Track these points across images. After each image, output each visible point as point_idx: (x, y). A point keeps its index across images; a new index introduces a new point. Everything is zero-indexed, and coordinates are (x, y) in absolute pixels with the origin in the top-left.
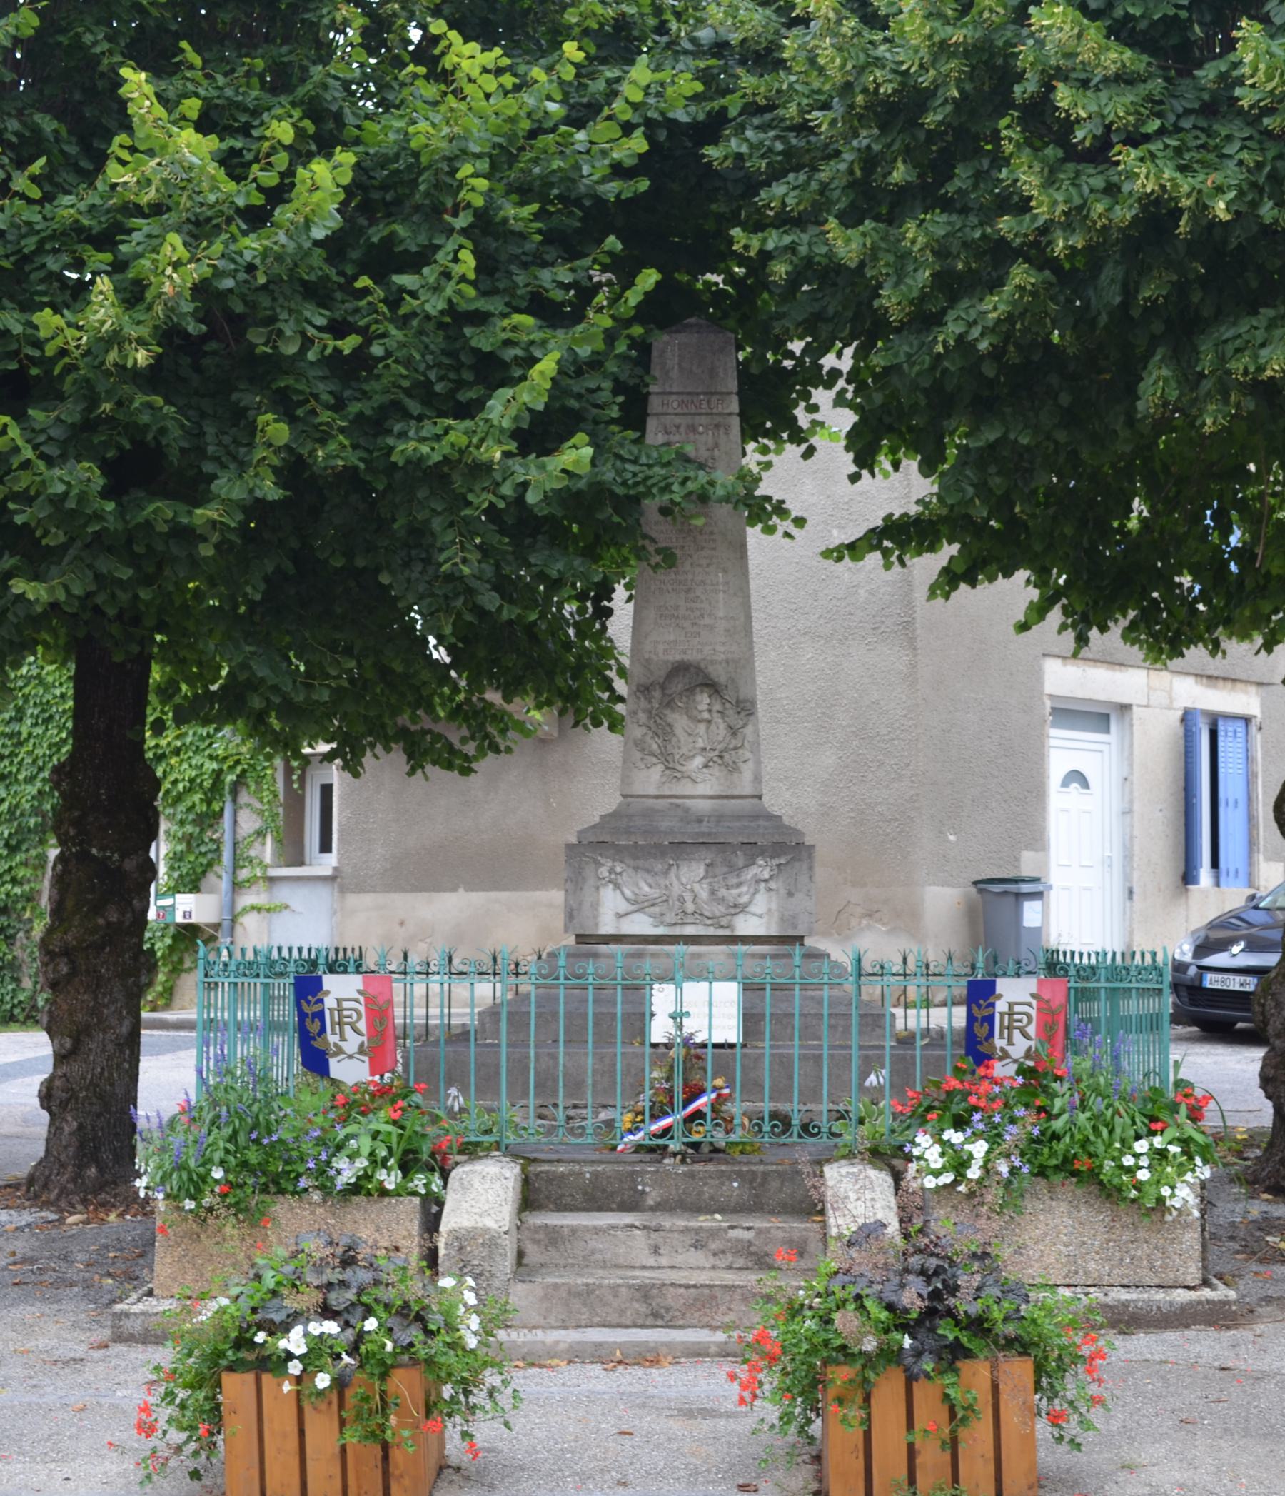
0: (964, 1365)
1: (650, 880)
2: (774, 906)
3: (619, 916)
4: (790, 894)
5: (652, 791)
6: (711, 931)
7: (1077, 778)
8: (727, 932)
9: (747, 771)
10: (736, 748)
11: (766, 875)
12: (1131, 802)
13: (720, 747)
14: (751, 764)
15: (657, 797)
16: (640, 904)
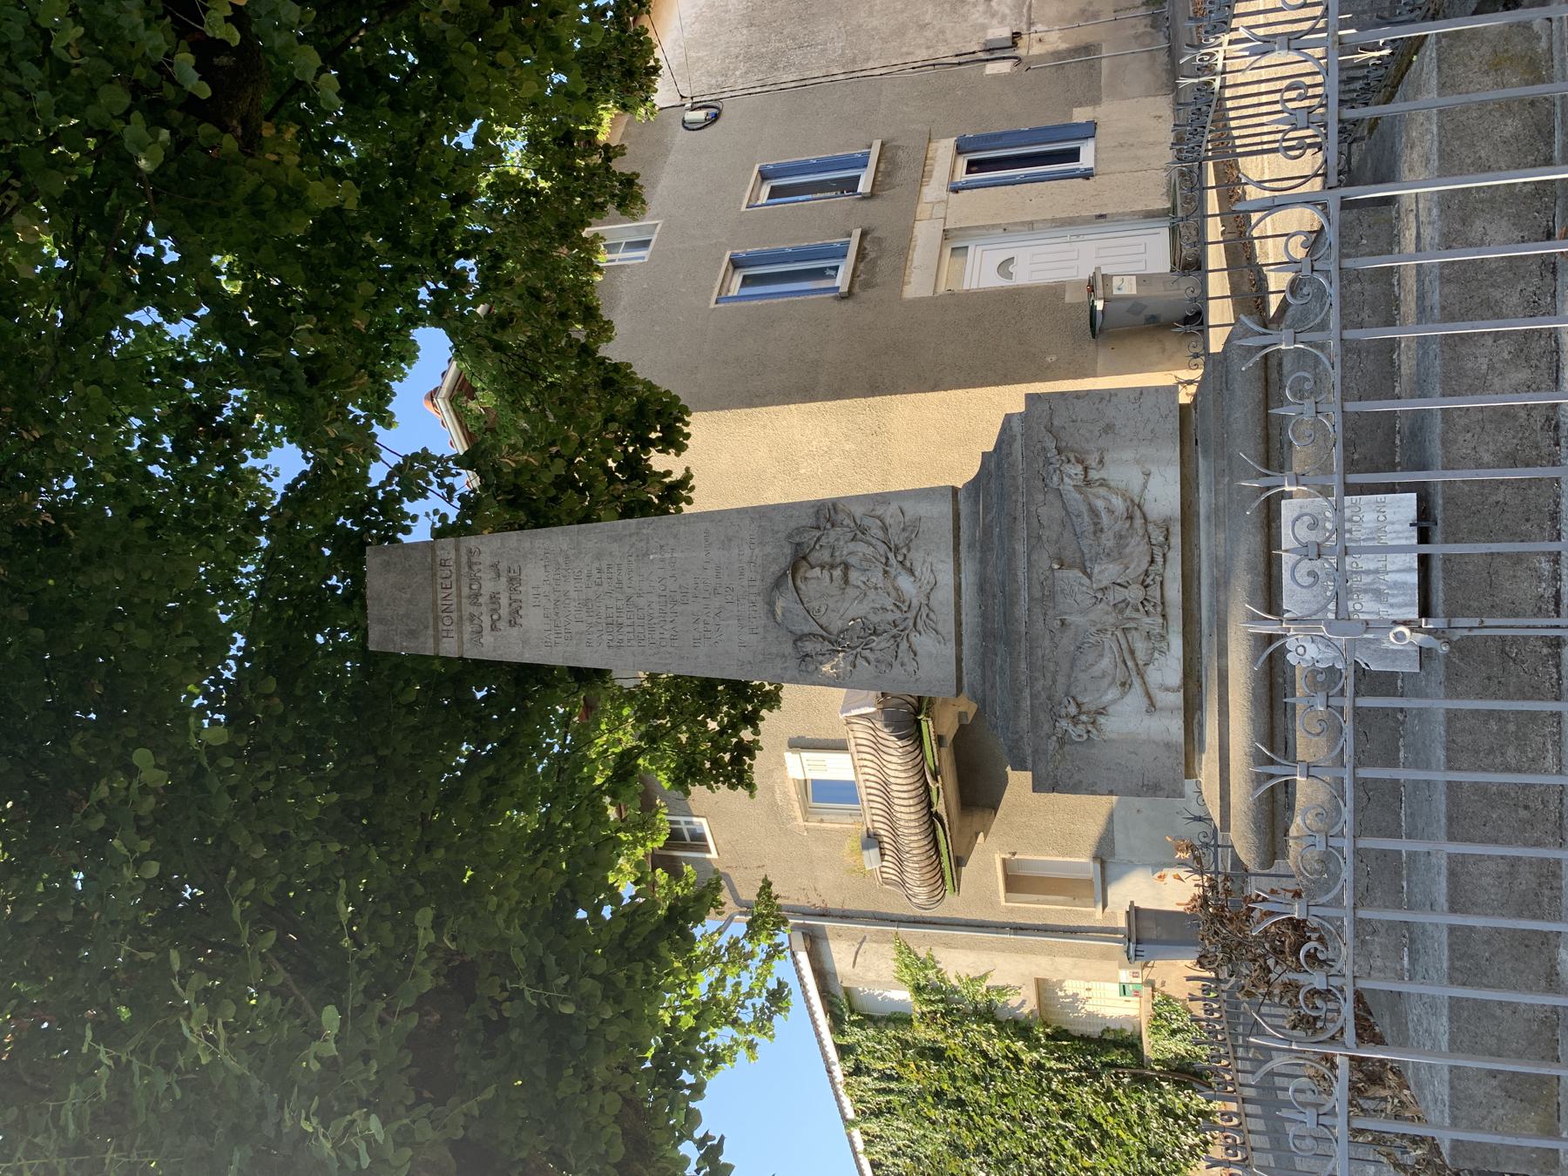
1: (1091, 658)
2: (1128, 455)
3: (1152, 706)
4: (1109, 429)
5: (950, 650)
6: (1175, 556)
7: (1004, 267)
8: (1176, 529)
9: (923, 509)
10: (885, 529)
12: (1023, 223)
13: (882, 548)
14: (907, 506)
15: (959, 642)
16: (1132, 672)
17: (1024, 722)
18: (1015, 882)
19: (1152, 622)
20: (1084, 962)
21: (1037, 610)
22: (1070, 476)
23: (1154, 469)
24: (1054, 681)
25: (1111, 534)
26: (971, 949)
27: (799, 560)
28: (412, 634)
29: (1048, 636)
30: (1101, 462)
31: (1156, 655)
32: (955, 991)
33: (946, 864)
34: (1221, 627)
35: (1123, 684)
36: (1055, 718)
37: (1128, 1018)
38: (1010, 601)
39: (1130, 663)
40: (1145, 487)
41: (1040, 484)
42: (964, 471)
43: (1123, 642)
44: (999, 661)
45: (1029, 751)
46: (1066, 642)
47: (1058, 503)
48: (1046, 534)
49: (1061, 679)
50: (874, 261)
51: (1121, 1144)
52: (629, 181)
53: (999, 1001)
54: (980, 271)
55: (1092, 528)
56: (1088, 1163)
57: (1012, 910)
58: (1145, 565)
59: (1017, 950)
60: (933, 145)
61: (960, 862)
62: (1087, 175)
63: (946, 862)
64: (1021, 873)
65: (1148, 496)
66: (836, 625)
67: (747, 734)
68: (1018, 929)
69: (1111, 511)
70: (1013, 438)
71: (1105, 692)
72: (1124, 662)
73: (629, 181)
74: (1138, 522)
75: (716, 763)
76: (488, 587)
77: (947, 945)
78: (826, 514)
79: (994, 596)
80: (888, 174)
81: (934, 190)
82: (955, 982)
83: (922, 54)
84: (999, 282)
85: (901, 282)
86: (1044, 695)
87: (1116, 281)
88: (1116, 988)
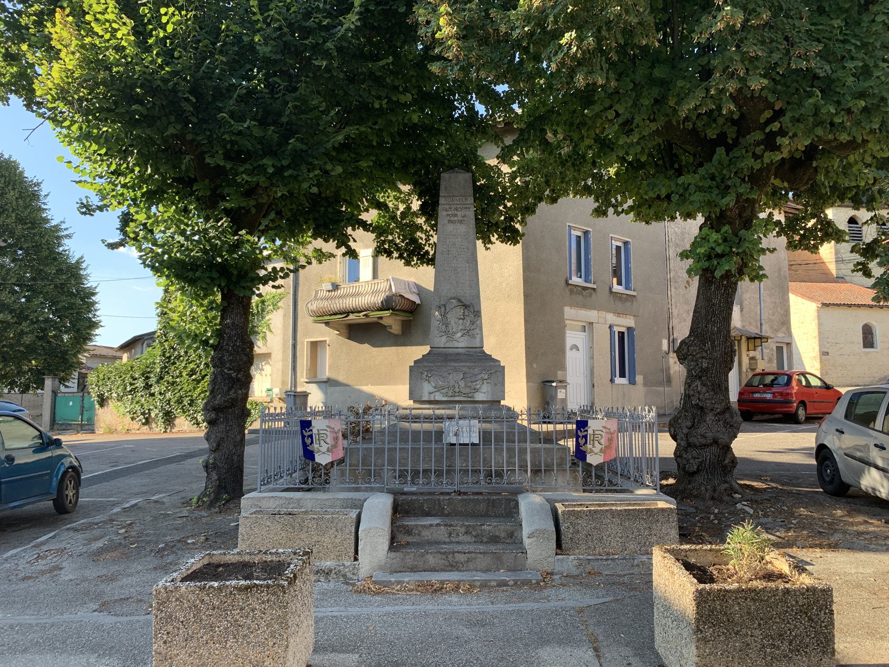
4: (496, 385)
6: (465, 399)
7: (575, 347)
9: (478, 340)
16: (438, 389)
18: (315, 346)
19: (450, 394)
20: (280, 373)
26: (284, 326)
27: (466, 306)
28: (446, 188)
32: (263, 318)
33: (326, 318)
37: (253, 392)
38: (455, 361)
42: (487, 350)
46: (445, 374)
50: (582, 294)
51: (195, 388)
52: (605, 214)
53: (260, 337)
54: (574, 337)
56: (184, 374)
57: (303, 344)
59: (284, 345)
60: (632, 317)
61: (327, 324)
62: (612, 381)
63: (326, 317)
64: (319, 348)
66: (448, 316)
67: (395, 255)
68: (294, 346)
73: (605, 214)
75: (384, 242)
76: (459, 213)
77: (285, 315)
78: (477, 314)
80: (620, 299)
81: (611, 318)
82: (267, 318)
83: (675, 312)
84: (568, 345)
85: (571, 306)
87: (563, 391)
88: (269, 387)
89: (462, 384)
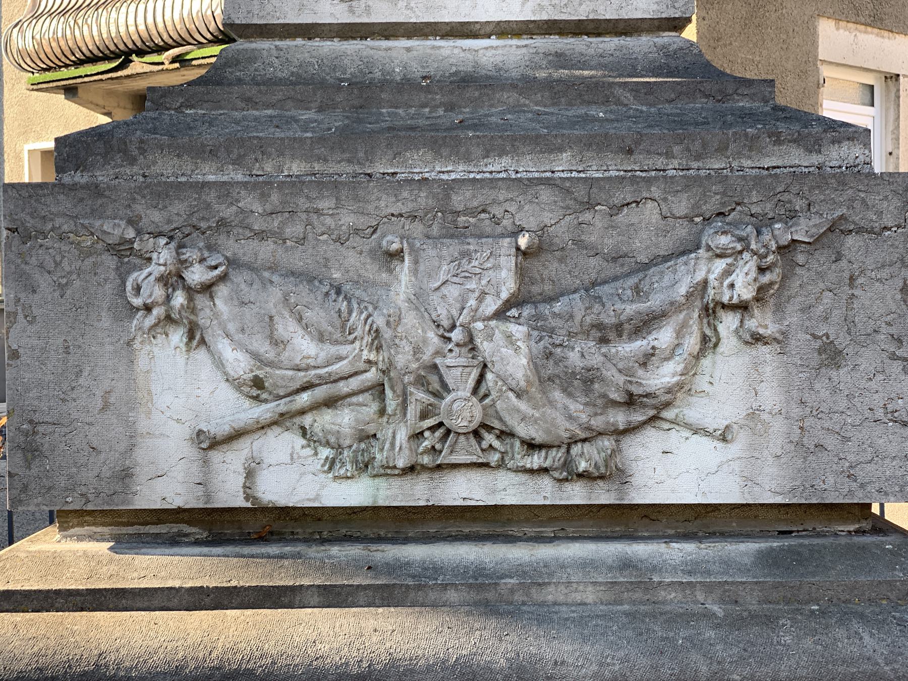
0: (271, 289)
2: (770, 397)
3: (211, 443)
4: (831, 355)
6: (544, 493)
8: (603, 496)
11: (743, 285)
16: (283, 400)
17: (167, 167)
19: (397, 441)
21: (424, 199)
22: (727, 272)
23: (735, 449)
24: (261, 235)
25: (596, 360)
29: (362, 222)
30: (757, 339)
31: (325, 452)
33: (65, 73)
34: (389, 593)
35: (258, 383)
36: (178, 238)
38: (444, 140)
39: (305, 398)
40: (697, 431)
41: (710, 208)
43: (354, 383)
44: (306, 115)
45: (102, 176)
46: (352, 262)
47: (665, 246)
48: (597, 219)
49: (266, 250)
55: (609, 319)
57: (18, 158)
58: (523, 430)
61: (70, 91)
65: (676, 438)
69: (647, 360)
70: (814, 147)
71: (239, 346)
72: (304, 389)
74: (620, 418)
79: (450, 107)
85: (839, 16)
86: (228, 212)
89: (511, 353)
